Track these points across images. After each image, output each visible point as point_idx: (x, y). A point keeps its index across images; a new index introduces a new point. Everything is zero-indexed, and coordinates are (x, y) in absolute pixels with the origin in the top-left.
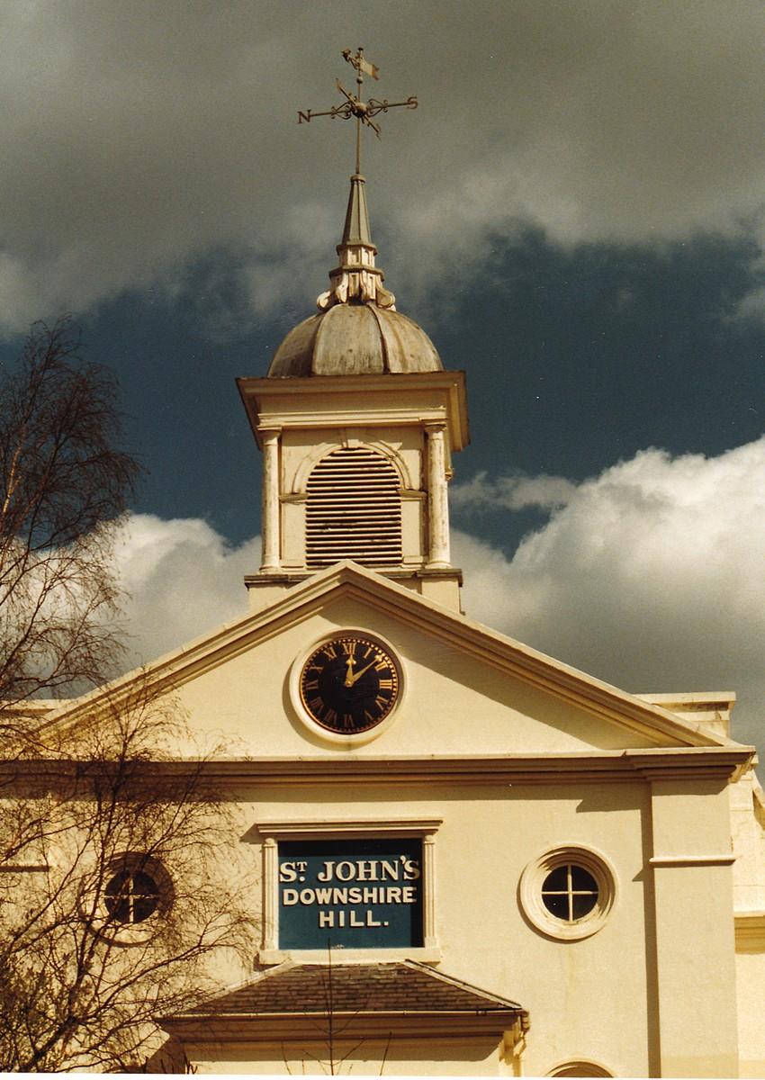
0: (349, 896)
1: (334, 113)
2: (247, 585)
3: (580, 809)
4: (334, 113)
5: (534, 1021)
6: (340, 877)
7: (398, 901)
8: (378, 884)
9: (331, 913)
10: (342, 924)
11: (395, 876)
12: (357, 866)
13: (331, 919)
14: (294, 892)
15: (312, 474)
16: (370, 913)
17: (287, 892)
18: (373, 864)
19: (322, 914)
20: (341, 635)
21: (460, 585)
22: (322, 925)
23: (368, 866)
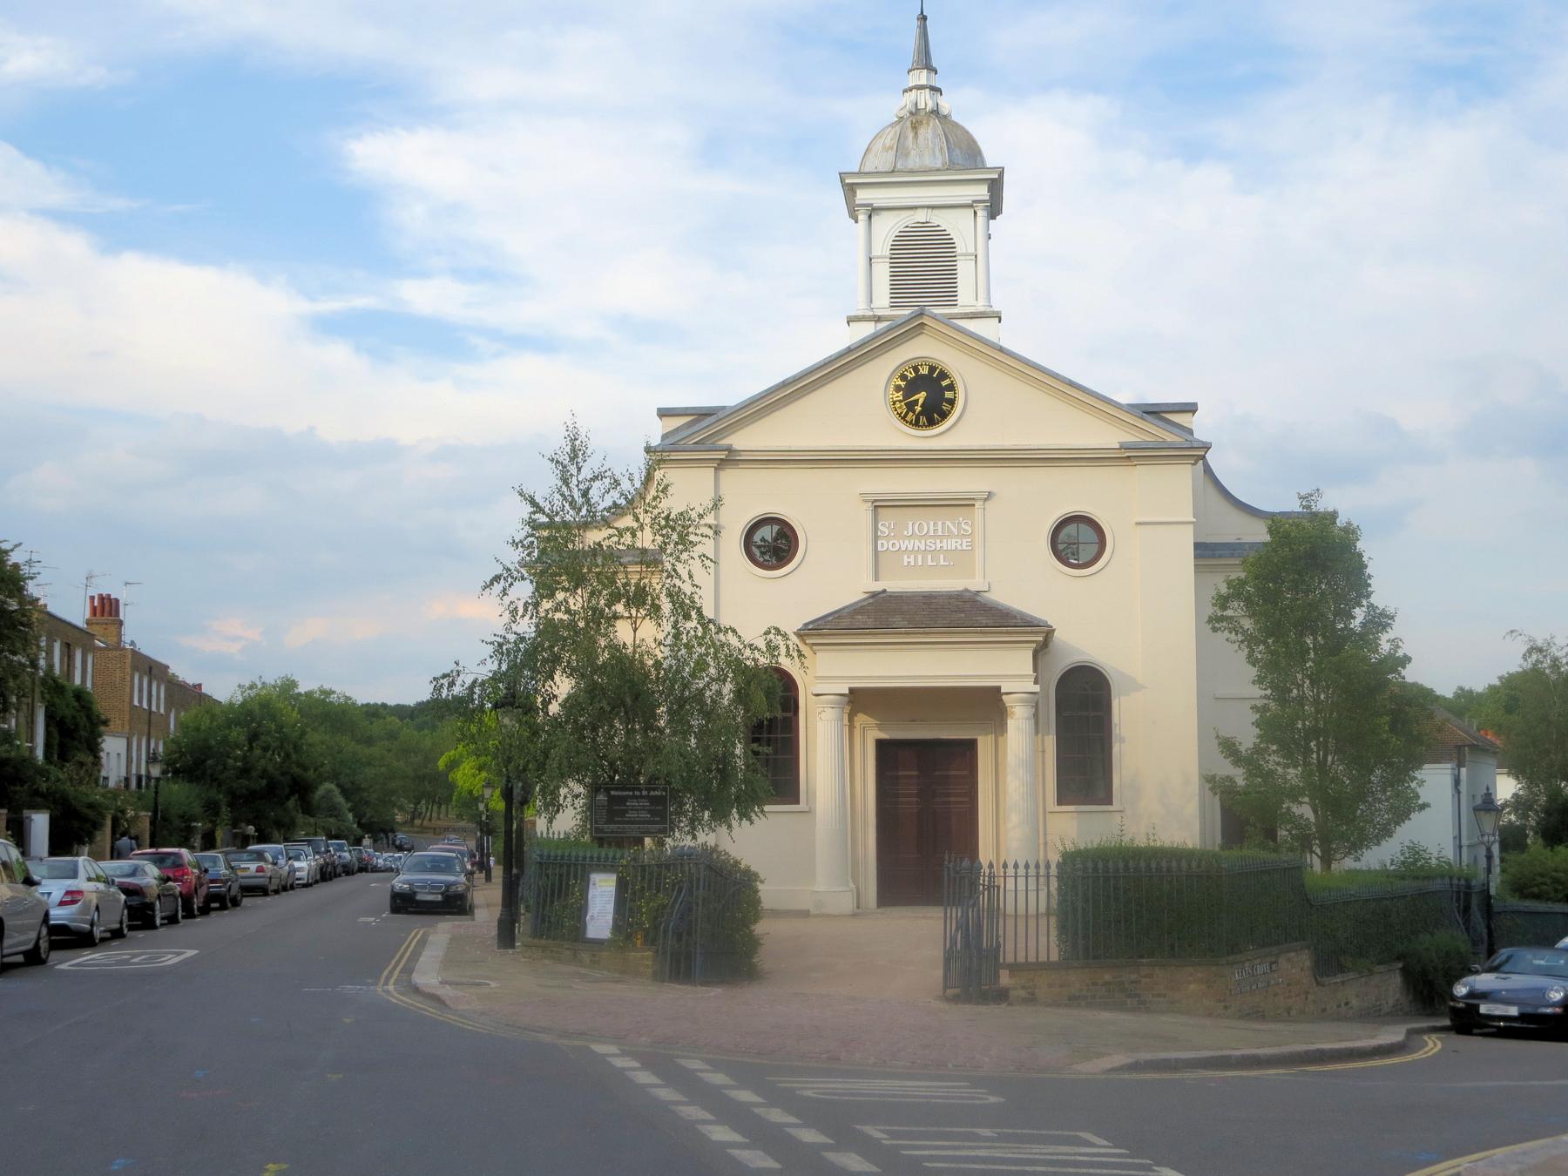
3: (762, 882)
7: (959, 548)
8: (941, 537)
9: (912, 556)
10: (920, 564)
11: (956, 531)
12: (928, 524)
15: (894, 241)
16: (942, 556)
19: (906, 557)
21: (1000, 322)
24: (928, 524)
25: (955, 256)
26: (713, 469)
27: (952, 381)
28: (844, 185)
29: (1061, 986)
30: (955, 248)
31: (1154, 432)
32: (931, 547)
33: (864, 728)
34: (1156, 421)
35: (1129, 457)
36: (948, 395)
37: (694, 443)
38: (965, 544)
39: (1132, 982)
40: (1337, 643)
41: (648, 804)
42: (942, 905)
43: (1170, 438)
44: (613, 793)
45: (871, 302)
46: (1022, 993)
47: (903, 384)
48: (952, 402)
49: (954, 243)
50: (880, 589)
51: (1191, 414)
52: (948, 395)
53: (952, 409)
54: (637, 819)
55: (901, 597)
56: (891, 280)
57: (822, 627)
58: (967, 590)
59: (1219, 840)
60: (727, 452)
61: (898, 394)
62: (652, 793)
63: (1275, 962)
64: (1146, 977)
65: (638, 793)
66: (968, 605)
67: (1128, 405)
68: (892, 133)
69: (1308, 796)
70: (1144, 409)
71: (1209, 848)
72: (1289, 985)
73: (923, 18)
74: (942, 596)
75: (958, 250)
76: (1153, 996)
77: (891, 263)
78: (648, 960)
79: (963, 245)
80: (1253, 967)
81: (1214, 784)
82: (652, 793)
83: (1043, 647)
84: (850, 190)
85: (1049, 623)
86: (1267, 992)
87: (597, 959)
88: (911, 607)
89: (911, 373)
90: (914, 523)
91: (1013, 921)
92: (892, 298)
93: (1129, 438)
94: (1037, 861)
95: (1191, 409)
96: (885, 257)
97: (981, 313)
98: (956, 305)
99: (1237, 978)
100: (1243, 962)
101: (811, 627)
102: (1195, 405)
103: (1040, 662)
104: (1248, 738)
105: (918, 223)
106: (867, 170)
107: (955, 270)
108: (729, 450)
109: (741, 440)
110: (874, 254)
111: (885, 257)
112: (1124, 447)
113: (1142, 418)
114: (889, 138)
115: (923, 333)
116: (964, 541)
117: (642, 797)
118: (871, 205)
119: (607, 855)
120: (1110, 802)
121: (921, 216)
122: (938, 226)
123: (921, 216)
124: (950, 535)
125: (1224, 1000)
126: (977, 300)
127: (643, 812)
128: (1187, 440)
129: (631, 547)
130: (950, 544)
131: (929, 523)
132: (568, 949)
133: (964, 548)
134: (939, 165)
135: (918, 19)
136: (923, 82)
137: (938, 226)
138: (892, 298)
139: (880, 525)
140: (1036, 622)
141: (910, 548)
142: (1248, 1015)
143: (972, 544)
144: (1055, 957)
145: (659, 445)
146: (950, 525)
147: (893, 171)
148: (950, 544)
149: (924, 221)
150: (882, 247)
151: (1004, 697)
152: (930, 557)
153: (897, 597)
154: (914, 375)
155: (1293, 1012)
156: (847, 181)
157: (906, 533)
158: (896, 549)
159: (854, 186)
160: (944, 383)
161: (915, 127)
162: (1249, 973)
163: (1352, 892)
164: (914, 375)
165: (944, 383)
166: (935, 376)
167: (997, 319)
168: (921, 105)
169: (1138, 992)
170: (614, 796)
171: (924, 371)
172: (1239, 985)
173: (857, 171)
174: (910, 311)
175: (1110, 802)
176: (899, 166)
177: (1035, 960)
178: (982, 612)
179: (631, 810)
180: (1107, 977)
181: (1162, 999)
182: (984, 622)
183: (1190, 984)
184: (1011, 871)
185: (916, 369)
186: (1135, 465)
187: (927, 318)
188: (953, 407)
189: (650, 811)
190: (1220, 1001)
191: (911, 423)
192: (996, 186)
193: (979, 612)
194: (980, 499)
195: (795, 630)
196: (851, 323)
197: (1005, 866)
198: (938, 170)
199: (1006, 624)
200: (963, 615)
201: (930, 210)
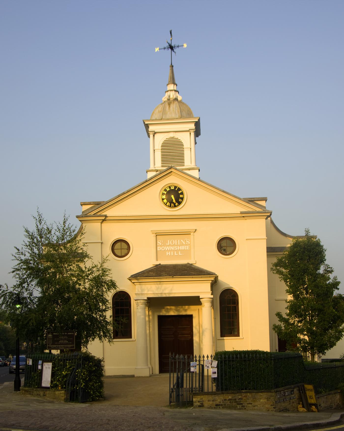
0: (174, 248)
8: (180, 245)
10: (172, 255)
12: (175, 241)
16: (180, 252)
19: (167, 252)
22: (167, 255)
24: (175, 241)
25: (184, 149)
26: (100, 223)
27: (182, 191)
29: (213, 401)
30: (183, 146)
31: (251, 208)
32: (176, 249)
33: (154, 311)
34: (252, 204)
35: (243, 217)
36: (181, 196)
37: (93, 214)
38: (187, 248)
39: (240, 399)
40: (315, 276)
41: (67, 337)
42: (169, 372)
43: (258, 210)
44: (54, 334)
45: (155, 165)
46: (199, 404)
47: (165, 193)
48: (182, 199)
49: (183, 144)
50: (158, 264)
51: (265, 201)
52: (181, 196)
53: (182, 201)
54: (63, 343)
55: (166, 266)
56: (161, 156)
57: (137, 276)
58: (188, 263)
59: (277, 348)
60: (105, 217)
62: (69, 334)
64: (244, 397)
66: (188, 269)
67: (243, 198)
68: (162, 106)
69: (306, 332)
70: (248, 200)
71: (274, 351)
73: (172, 66)
74: (180, 265)
76: (247, 404)
78: (62, 394)
80: (284, 393)
81: (275, 328)
82: (69, 334)
83: (215, 283)
85: (216, 274)
86: (290, 401)
87: (45, 394)
88: (169, 269)
89: (168, 189)
90: (170, 240)
92: (162, 163)
94: (200, 355)
95: (265, 199)
96: (159, 149)
97: (192, 168)
98: (184, 166)
99: (278, 397)
100: (280, 391)
101: (133, 276)
102: (266, 198)
103: (214, 288)
104: (285, 312)
105: (171, 137)
106: (153, 119)
108: (106, 216)
109: (110, 213)
110: (155, 148)
111: (159, 149)
112: (242, 213)
113: (248, 203)
114: (160, 108)
115: (171, 175)
116: (187, 246)
118: (154, 131)
119: (39, 356)
120: (239, 336)
121: (171, 135)
122: (177, 138)
123: (171, 135)
124: (182, 245)
125: (274, 405)
126: (191, 163)
127: (66, 340)
128: (264, 210)
130: (182, 248)
131: (176, 240)
132: (35, 391)
133: (187, 249)
134: (177, 117)
135: (170, 67)
136: (172, 88)
137: (177, 138)
138: (162, 163)
139: (158, 241)
140: (211, 273)
141: (169, 249)
142: (283, 410)
143: (190, 247)
144: (214, 388)
145: (81, 215)
146: (183, 242)
147: (161, 119)
149: (173, 137)
151: (201, 300)
152: (175, 252)
153: (164, 266)
154: (169, 189)
156: (146, 123)
158: (164, 250)
159: (148, 125)
160: (180, 192)
161: (169, 104)
162: (283, 395)
163: (321, 365)
164: (169, 189)
165: (180, 192)
166: (176, 190)
168: (171, 97)
169: (241, 403)
171: (173, 188)
173: (150, 119)
175: (239, 336)
176: (164, 118)
177: (207, 391)
178: (193, 270)
179: (61, 340)
180: (230, 397)
181: (250, 405)
182: (193, 274)
183: (261, 399)
184: (206, 358)
185: (170, 187)
186: (246, 219)
187: (173, 169)
188: (183, 200)
189: (68, 340)
190: (272, 405)
191: (168, 206)
192: (197, 124)
193: (192, 271)
194: (192, 232)
195: (128, 278)
196: (148, 172)
197: (204, 357)
198: (177, 118)
199: (201, 274)
200: (186, 272)
201: (175, 133)
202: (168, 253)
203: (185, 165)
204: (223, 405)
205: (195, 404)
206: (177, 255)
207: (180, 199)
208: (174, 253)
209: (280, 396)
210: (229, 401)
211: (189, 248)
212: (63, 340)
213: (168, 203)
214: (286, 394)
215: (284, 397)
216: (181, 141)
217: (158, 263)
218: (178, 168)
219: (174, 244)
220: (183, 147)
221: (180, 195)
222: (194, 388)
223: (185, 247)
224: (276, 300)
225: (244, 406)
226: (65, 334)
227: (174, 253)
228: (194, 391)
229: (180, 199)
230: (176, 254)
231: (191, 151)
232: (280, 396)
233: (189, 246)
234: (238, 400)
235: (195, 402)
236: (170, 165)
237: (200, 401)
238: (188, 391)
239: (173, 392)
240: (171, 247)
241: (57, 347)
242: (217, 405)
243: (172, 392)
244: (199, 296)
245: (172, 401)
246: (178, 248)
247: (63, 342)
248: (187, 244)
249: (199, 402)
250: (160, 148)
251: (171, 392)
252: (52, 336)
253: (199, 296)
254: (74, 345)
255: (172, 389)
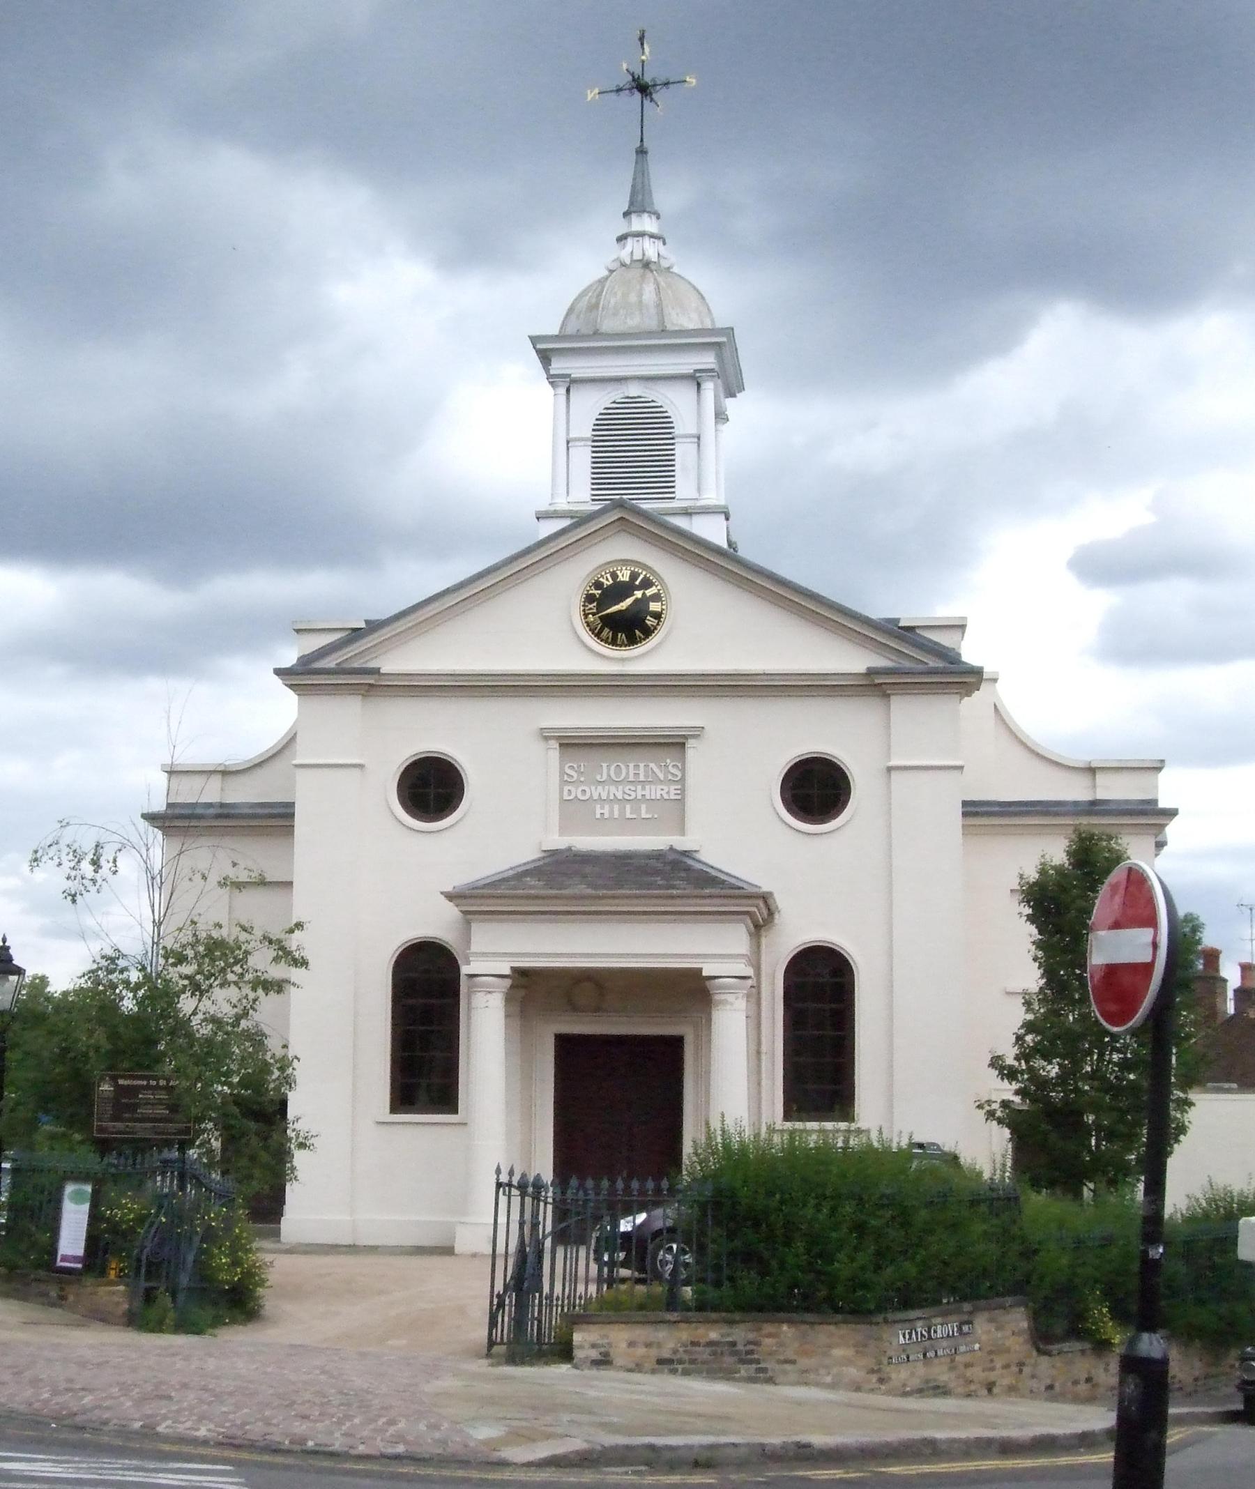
0: (624, 793)
1: (619, 90)
2: (538, 518)
4: (619, 90)
5: (1069, 553)
6: (623, 767)
10: (616, 816)
11: (661, 776)
13: (606, 811)
14: (573, 789)
15: (597, 420)
17: (566, 788)
18: (642, 765)
20: (599, 570)
22: (598, 816)
23: (637, 767)
28: (539, 352)
30: (673, 428)
32: (630, 795)
39: (749, 1343)
44: (121, 1082)
46: (594, 1354)
49: (672, 422)
53: (658, 624)
61: (591, 606)
63: (969, 1322)
65: (154, 1083)
72: (991, 1352)
75: (677, 431)
77: (593, 447)
79: (683, 423)
84: (545, 357)
89: (607, 579)
91: (503, 1262)
92: (593, 489)
93: (880, 662)
98: (674, 498)
105: (628, 397)
107: (673, 455)
108: (376, 671)
112: (871, 672)
116: (673, 787)
117: (158, 1087)
118: (569, 376)
121: (634, 390)
123: (634, 390)
125: (879, 1371)
127: (161, 1107)
129: (1107, 847)
130: (654, 792)
133: (673, 797)
137: (653, 401)
146: (656, 770)
148: (654, 792)
150: (584, 427)
154: (611, 582)
155: (995, 1390)
157: (598, 778)
158: (571, 798)
162: (922, 1335)
164: (611, 582)
167: (723, 517)
170: (122, 1086)
172: (904, 1351)
173: (556, 333)
174: (599, 507)
180: (714, 1335)
188: (659, 621)
190: (872, 1371)
202: (602, 808)
203: (678, 495)
204: (684, 1363)
205: (579, 1354)
206: (634, 816)
207: (648, 618)
208: (622, 811)
209: (910, 1338)
210: (708, 1350)
211: (679, 792)
212: (153, 1104)
213: (607, 630)
214: (935, 1332)
215: (927, 1343)
216: (666, 412)
217: (558, 842)
218: (645, 506)
219: (622, 777)
220: (670, 433)
221: (651, 604)
222: (580, 1298)
223: (662, 790)
224: (1008, 993)
225: (764, 1370)
226: (158, 1083)
227: (622, 811)
228: (580, 1305)
229: (648, 618)
230: (647, 813)
231: (699, 446)
232: (910, 1338)
233: (679, 787)
234: (745, 1345)
235: (581, 1347)
236: (618, 497)
237: (598, 1342)
238: (557, 1306)
239: (501, 1305)
240: (613, 789)
241: (128, 1129)
242: (661, 1362)
243: (498, 1309)
244: (700, 970)
245: (499, 1340)
246: (640, 792)
247: (151, 1111)
248: (670, 777)
249: (594, 1346)
250: (588, 433)
251: (495, 1307)
252: (112, 1089)
253: (700, 970)
254: (97, 1126)
255: (499, 1296)
